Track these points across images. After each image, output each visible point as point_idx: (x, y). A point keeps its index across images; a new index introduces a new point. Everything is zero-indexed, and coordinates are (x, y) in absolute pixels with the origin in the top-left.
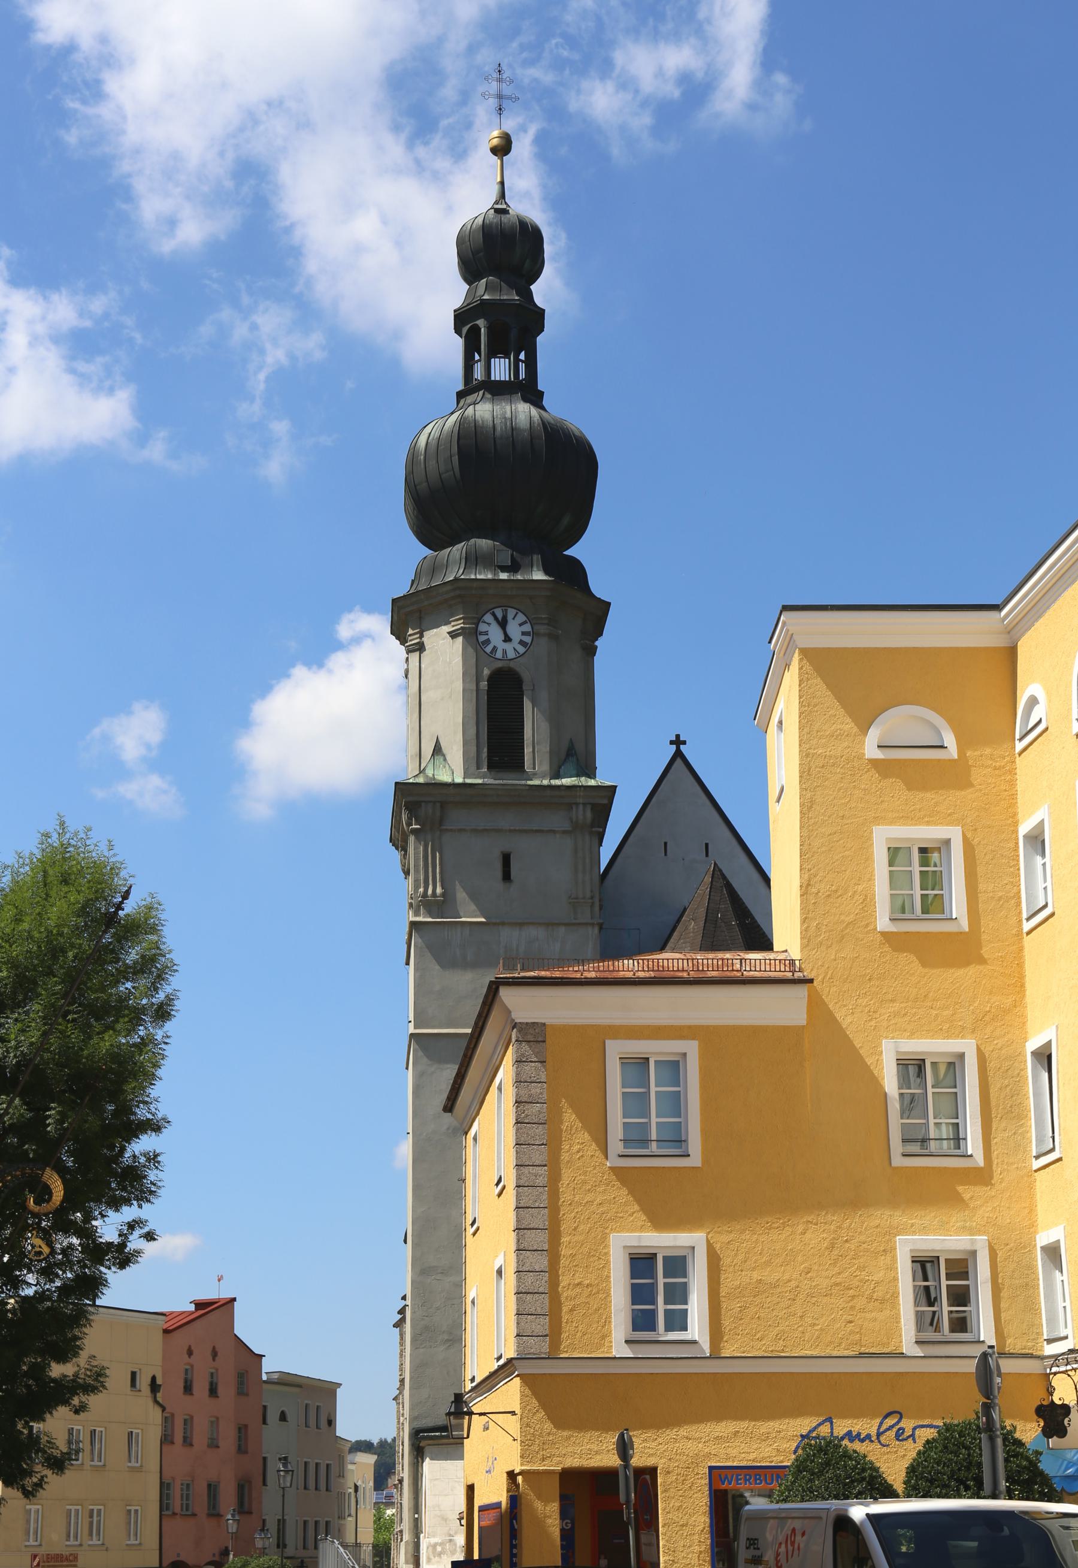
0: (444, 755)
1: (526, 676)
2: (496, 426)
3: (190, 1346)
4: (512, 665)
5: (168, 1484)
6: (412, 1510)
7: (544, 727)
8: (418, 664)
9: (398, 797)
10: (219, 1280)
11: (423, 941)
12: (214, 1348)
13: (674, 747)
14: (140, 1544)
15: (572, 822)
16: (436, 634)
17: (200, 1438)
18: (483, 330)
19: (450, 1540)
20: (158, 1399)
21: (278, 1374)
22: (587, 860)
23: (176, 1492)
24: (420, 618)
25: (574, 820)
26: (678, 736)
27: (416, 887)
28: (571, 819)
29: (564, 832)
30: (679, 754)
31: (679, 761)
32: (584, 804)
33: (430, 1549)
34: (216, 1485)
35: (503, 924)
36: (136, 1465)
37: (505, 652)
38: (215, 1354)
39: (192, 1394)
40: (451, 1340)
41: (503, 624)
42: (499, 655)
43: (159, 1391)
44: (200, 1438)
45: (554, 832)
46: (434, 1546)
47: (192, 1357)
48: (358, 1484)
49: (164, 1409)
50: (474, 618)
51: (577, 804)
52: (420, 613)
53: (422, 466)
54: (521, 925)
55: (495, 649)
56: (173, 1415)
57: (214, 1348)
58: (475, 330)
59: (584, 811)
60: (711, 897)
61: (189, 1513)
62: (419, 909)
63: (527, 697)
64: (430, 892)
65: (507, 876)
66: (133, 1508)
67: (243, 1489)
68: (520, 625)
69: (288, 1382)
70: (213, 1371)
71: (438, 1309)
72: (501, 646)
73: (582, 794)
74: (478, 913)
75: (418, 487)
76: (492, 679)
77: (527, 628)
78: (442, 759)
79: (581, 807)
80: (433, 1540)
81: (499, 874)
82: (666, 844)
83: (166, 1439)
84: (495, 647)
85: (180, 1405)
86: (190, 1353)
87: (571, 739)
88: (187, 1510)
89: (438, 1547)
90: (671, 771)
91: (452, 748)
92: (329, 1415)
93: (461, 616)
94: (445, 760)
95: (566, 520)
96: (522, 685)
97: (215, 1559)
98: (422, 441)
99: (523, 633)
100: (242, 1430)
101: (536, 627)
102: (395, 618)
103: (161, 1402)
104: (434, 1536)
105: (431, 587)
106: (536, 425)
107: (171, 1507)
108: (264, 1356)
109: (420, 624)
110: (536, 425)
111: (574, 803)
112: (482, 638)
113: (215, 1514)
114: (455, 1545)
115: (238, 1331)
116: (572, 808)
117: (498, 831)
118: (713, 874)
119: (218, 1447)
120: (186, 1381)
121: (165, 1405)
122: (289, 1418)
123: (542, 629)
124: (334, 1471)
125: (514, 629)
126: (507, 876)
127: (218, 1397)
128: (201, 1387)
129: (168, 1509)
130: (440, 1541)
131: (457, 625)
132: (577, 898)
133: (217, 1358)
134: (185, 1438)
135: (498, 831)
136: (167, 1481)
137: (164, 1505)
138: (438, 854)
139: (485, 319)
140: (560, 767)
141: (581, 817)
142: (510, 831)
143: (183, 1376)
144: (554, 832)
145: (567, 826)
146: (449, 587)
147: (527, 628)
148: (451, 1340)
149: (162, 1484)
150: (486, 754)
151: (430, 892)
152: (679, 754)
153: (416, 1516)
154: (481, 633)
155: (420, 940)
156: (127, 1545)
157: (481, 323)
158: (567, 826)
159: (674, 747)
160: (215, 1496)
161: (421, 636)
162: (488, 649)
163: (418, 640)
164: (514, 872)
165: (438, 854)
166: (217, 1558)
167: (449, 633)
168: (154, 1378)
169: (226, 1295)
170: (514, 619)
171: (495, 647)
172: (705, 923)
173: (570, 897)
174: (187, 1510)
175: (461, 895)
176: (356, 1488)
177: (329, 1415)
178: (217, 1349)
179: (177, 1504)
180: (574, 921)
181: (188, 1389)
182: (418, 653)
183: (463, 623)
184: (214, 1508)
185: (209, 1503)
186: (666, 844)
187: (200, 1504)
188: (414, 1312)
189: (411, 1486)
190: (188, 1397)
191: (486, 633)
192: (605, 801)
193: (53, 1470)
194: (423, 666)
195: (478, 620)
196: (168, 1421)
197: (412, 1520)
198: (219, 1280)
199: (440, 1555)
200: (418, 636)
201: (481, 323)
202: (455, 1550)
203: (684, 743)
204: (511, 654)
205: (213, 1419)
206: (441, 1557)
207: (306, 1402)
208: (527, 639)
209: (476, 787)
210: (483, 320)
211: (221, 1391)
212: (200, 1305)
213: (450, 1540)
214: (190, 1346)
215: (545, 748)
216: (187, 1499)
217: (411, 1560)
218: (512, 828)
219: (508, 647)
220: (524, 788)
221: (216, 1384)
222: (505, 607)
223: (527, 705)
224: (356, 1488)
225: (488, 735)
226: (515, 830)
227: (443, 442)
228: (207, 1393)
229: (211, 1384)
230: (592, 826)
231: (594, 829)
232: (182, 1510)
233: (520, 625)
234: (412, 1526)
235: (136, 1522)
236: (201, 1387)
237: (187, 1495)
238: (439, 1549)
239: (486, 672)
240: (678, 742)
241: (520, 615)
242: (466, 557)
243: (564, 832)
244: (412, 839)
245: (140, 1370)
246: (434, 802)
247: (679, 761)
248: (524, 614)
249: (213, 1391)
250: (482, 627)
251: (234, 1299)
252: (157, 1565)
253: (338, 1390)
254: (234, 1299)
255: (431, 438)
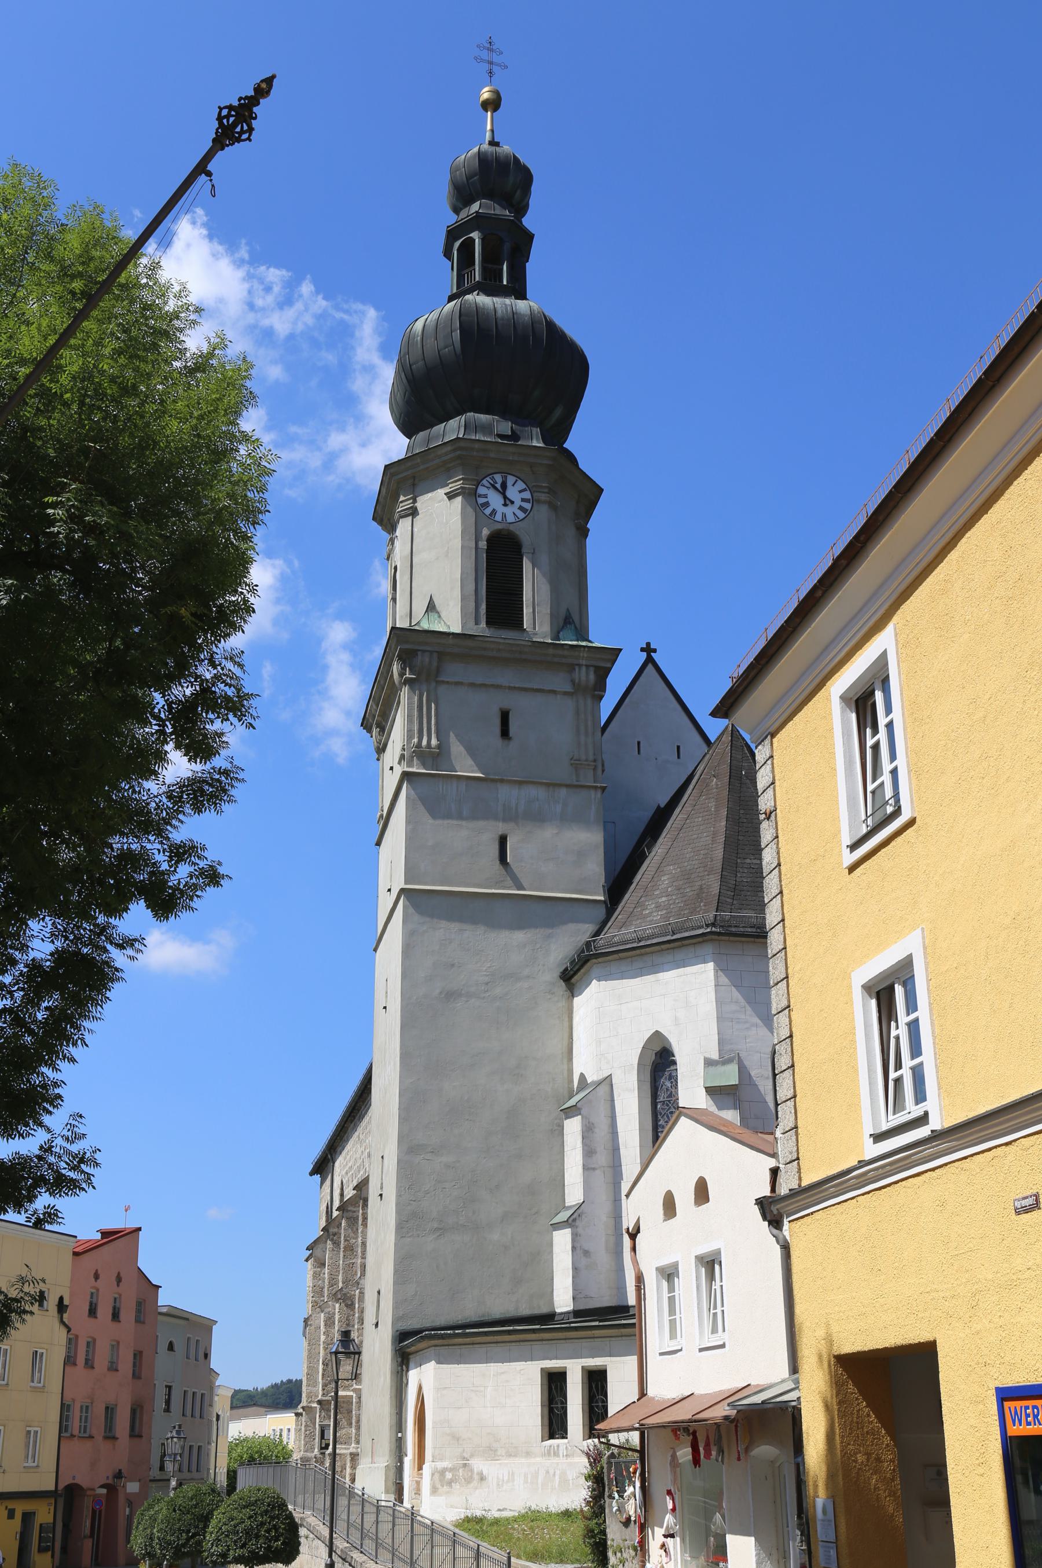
0: (438, 613)
1: (526, 540)
2: (497, 309)
3: (97, 1271)
4: (512, 528)
5: (69, 1406)
6: (394, 1428)
7: (545, 589)
8: (410, 528)
9: (390, 649)
10: (126, 1210)
11: (416, 794)
12: (119, 1274)
13: (644, 655)
14: (38, 1466)
15: (574, 685)
16: (431, 498)
17: (101, 1360)
18: (477, 241)
19: (465, 1465)
20: (64, 1320)
21: (167, 1307)
22: (590, 723)
23: (76, 1414)
24: (414, 485)
25: (577, 681)
26: (648, 644)
27: (410, 737)
28: (573, 681)
29: (565, 693)
30: (650, 660)
31: (650, 666)
32: (587, 666)
33: (437, 1476)
34: (112, 1409)
35: (502, 781)
36: (39, 1385)
37: (504, 516)
38: (119, 1279)
39: (96, 1317)
40: (441, 1229)
41: (503, 490)
42: (498, 517)
43: (66, 1312)
44: (101, 1360)
45: (554, 692)
46: (443, 1472)
47: (98, 1281)
48: (219, 1414)
49: (69, 1330)
50: (475, 480)
51: (580, 665)
52: (414, 480)
53: (419, 345)
54: (520, 783)
55: (494, 512)
56: (77, 1337)
57: (119, 1274)
58: (467, 248)
59: (587, 674)
60: (733, 755)
61: (87, 1435)
62: (412, 760)
63: (526, 557)
64: (424, 742)
65: (505, 733)
66: (32, 1429)
67: (137, 1411)
68: (520, 492)
69: (177, 1315)
70: (116, 1296)
71: (427, 1192)
72: (501, 509)
73: (585, 655)
74: (476, 768)
75: (414, 367)
76: (490, 540)
77: (527, 495)
78: (436, 616)
79: (584, 669)
80: (441, 1465)
81: (497, 729)
82: (639, 743)
83: (69, 1361)
84: (494, 510)
85: (84, 1326)
86: (97, 1276)
87: (568, 610)
88: (85, 1432)
89: (447, 1473)
90: (643, 675)
91: (448, 605)
92: (206, 1349)
93: (461, 477)
94: (440, 616)
95: (558, 412)
96: (521, 549)
97: (108, 1482)
98: (419, 325)
99: (523, 500)
100: (138, 1355)
101: (535, 494)
102: (384, 491)
103: (67, 1323)
104: (441, 1460)
105: (429, 449)
106: (536, 312)
107: (70, 1430)
108: (161, 1287)
109: (414, 491)
110: (536, 312)
111: (577, 665)
112: (481, 501)
113: (110, 1436)
114: (472, 1471)
115: (142, 1264)
116: (574, 669)
117: (498, 687)
118: (732, 733)
119: (118, 1371)
120: (91, 1304)
121: (70, 1326)
122: (176, 1348)
123: (543, 497)
124: (207, 1398)
125: (512, 493)
126: (505, 733)
127: (120, 1321)
128: (104, 1311)
129: (66, 1431)
130: (450, 1466)
131: (455, 485)
132: (579, 760)
133: (121, 1284)
134: (87, 1360)
135: (498, 687)
136: (67, 1403)
137: (63, 1427)
138: (433, 705)
139: (479, 231)
140: (559, 633)
141: (583, 678)
142: (510, 688)
143: (89, 1297)
144: (554, 692)
145: (568, 688)
146: (449, 448)
147: (527, 495)
148: (441, 1229)
149: (62, 1405)
150: (485, 611)
151: (424, 742)
152: (650, 660)
153: (400, 1435)
154: (480, 496)
155: (412, 792)
156: (24, 1467)
157: (475, 235)
158: (568, 688)
159: (644, 655)
160: (112, 1418)
161: (415, 501)
162: (488, 511)
163: (412, 505)
164: (513, 729)
165: (433, 705)
166: (110, 1481)
167: (445, 494)
168: (61, 1299)
169: (132, 1225)
170: (513, 485)
171: (494, 510)
172: (730, 778)
173: (571, 759)
174: (85, 1432)
175: (457, 749)
176: (218, 1417)
177: (206, 1349)
178: (121, 1275)
179: (75, 1426)
180: (577, 783)
181: (92, 1312)
182: (410, 518)
183: (462, 484)
184: (110, 1430)
185: (106, 1426)
186: (639, 743)
187: (97, 1428)
188: (400, 1196)
189: (394, 1399)
190: (92, 1320)
191: (485, 496)
192: (609, 665)
193: (156, 911)
194: (415, 530)
195: (478, 483)
196: (72, 1342)
197: (394, 1440)
198: (126, 1210)
199: (450, 1483)
200: (411, 501)
201: (475, 235)
202: (471, 1477)
203: (655, 651)
204: (511, 518)
205: (114, 1343)
206: (451, 1487)
207: (188, 1335)
208: (527, 506)
209: (476, 638)
210: (477, 232)
211: (123, 1315)
212: (105, 1234)
213: (465, 1465)
214: (97, 1271)
215: (545, 610)
216: (86, 1422)
217: (393, 1488)
218: (512, 685)
219: (509, 511)
220: (526, 643)
221: (119, 1309)
222: (505, 474)
223: (527, 565)
224: (218, 1417)
225: (487, 592)
226: (515, 688)
227: (442, 321)
228: (110, 1317)
229: (114, 1308)
230: (595, 689)
231: (596, 693)
232: (80, 1432)
233: (520, 492)
234: (394, 1446)
235: (35, 1442)
236: (104, 1311)
237: (86, 1417)
238: (449, 1476)
239: (485, 532)
240: (648, 649)
241: (520, 482)
242: (465, 424)
243: (565, 693)
244: (406, 690)
245: (49, 1289)
246: (431, 652)
247: (650, 666)
248: (523, 482)
249: (116, 1316)
250: (481, 490)
251: (140, 1229)
252: (53, 1489)
253: (214, 1327)
254: (140, 1229)
255: (428, 321)
